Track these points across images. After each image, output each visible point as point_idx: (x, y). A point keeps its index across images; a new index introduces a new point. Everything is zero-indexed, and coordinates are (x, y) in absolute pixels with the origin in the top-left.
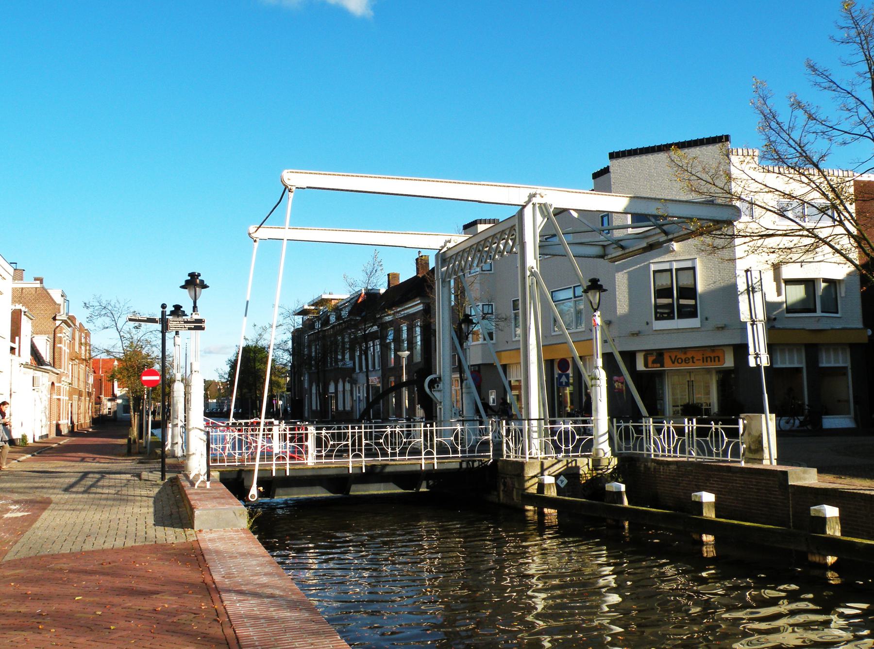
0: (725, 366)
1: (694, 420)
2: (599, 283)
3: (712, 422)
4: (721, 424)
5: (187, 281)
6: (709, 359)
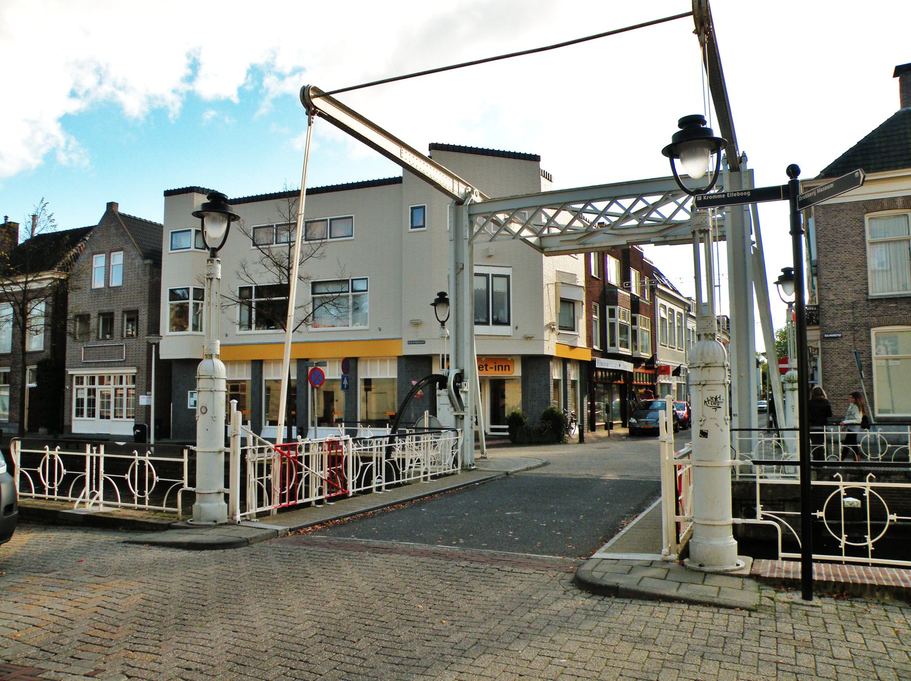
0: (513, 375)
1: (102, 448)
2: (446, 297)
3: (47, 447)
4: (59, 450)
5: (780, 277)
6: (500, 368)
